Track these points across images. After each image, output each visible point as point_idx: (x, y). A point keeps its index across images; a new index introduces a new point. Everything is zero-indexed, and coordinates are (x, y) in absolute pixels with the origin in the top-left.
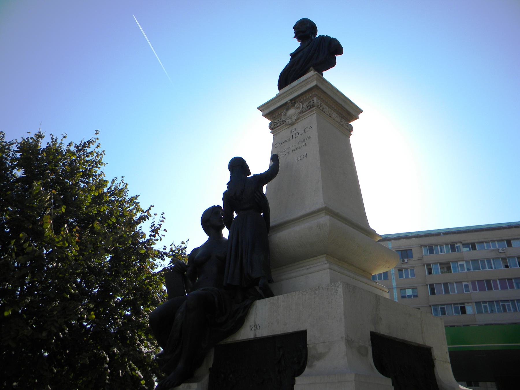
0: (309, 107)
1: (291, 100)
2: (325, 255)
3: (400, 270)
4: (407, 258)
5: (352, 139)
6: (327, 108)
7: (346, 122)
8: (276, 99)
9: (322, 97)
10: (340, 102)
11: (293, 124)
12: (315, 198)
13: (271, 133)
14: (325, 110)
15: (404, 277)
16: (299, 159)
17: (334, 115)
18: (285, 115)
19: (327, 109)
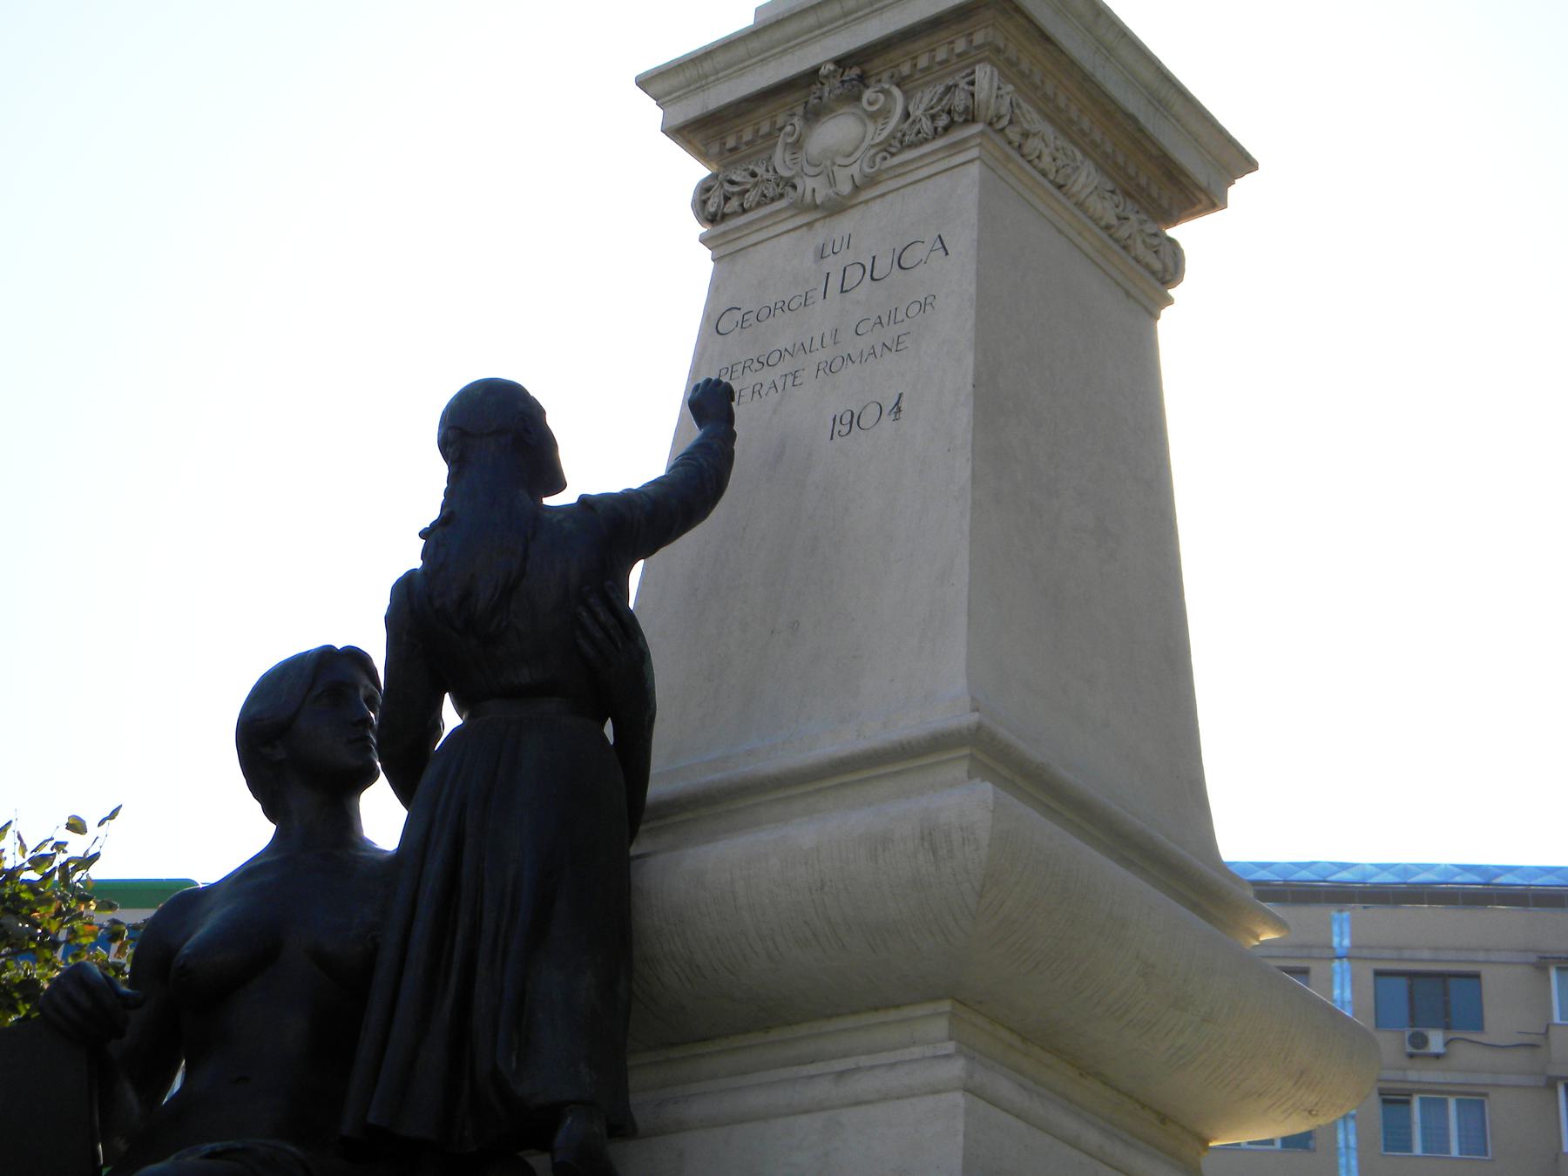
0: (943, 121)
1: (841, 62)
2: (946, 1005)
3: (1394, 1100)
4: (1447, 1027)
5: (1169, 326)
6: (1048, 130)
7: (1150, 228)
8: (755, 44)
9: (1025, 66)
10: (1131, 102)
11: (835, 208)
12: (922, 676)
13: (704, 240)
14: (1032, 145)
15: (1418, 1149)
16: (855, 420)
17: (1086, 178)
18: (797, 146)
19: (1046, 140)
